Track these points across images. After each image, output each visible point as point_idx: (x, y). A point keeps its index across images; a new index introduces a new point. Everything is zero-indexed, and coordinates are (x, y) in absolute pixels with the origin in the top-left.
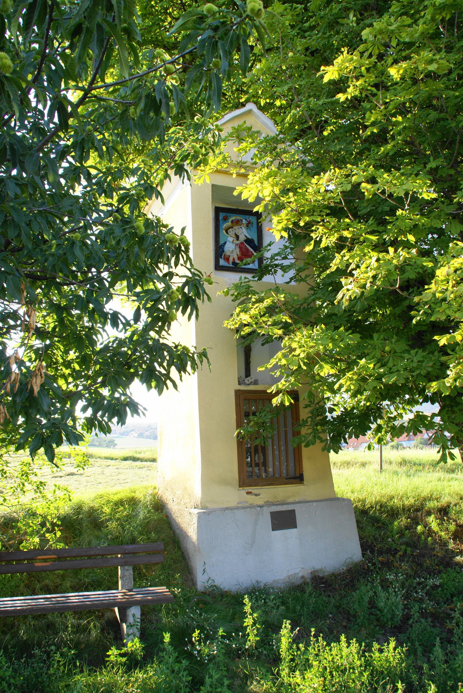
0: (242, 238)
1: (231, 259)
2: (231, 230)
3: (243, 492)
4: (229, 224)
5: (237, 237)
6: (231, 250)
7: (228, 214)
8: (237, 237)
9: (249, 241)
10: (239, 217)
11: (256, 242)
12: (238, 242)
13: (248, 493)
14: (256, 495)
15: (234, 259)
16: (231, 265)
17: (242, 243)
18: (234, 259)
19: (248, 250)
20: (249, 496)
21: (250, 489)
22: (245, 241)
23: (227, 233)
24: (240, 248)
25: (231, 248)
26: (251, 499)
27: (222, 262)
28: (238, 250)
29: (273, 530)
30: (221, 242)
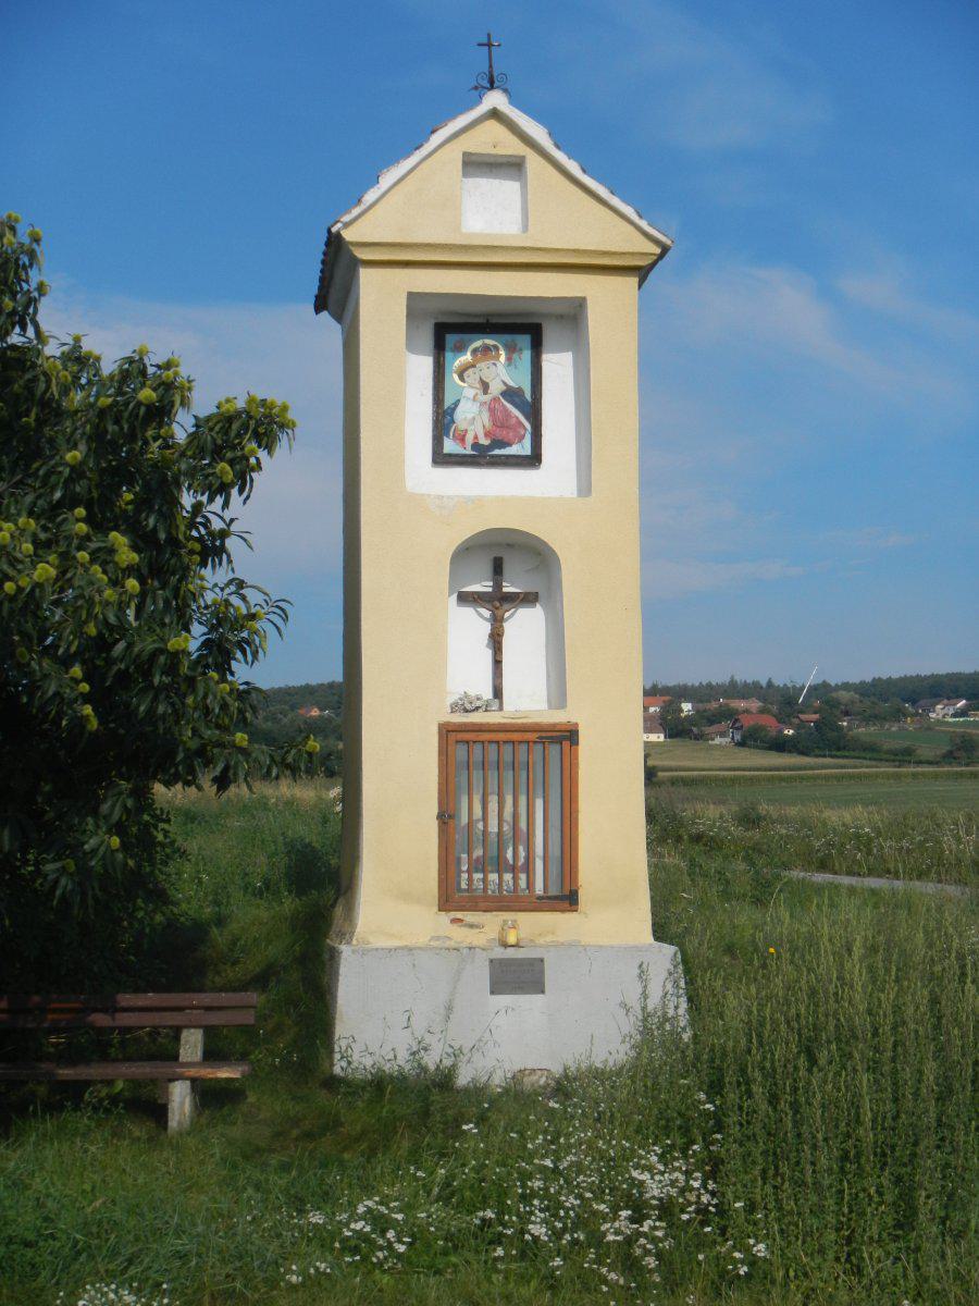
0: (496, 388)
1: (469, 439)
2: (470, 371)
3: (445, 918)
4: (467, 357)
5: (485, 387)
6: (470, 416)
7: (466, 337)
8: (485, 387)
9: (511, 394)
10: (489, 342)
11: (528, 396)
12: (487, 398)
13: (454, 921)
14: (471, 926)
15: (476, 437)
16: (469, 451)
17: (495, 399)
18: (476, 437)
19: (508, 414)
20: (455, 927)
21: (459, 915)
22: (504, 394)
23: (462, 379)
24: (492, 411)
25: (472, 417)
26: (460, 935)
27: (450, 446)
28: (486, 417)
29: (492, 993)
30: (448, 402)
